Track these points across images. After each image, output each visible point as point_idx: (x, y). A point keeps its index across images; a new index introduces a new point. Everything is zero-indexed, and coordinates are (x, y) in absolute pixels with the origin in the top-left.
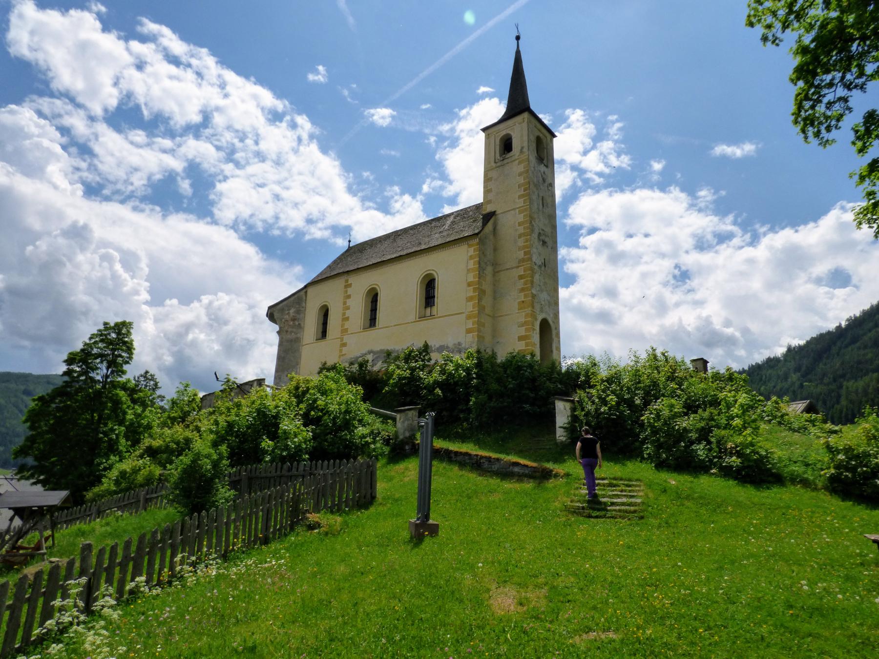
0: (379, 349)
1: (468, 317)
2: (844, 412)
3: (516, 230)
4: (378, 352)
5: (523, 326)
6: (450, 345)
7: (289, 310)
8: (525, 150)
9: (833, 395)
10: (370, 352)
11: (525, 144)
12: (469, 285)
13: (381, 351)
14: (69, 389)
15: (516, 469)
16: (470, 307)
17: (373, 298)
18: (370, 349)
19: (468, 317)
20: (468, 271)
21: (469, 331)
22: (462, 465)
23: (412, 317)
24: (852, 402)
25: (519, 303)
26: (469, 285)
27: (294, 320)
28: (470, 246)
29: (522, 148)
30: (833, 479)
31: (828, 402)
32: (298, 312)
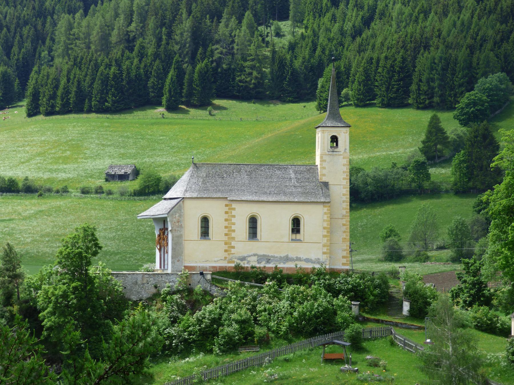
0: (262, 254)
1: (324, 246)
2: (61, 86)
3: (341, 198)
4: (261, 256)
5: (344, 251)
6: (313, 259)
7: (176, 214)
8: (348, 151)
9: (25, 31)
10: (255, 255)
11: (348, 148)
12: (324, 228)
13: (264, 256)
14: (313, 313)
15: (412, 327)
16: (325, 240)
17: (253, 222)
18: (255, 253)
19: (324, 246)
20: (324, 220)
21: (324, 253)
22: (402, 327)
23: (286, 239)
24: (77, 63)
25: (343, 239)
26: (324, 228)
27: (178, 222)
28: (324, 207)
29: (346, 149)
30: (477, 325)
31: (15, 49)
32: (180, 216)
